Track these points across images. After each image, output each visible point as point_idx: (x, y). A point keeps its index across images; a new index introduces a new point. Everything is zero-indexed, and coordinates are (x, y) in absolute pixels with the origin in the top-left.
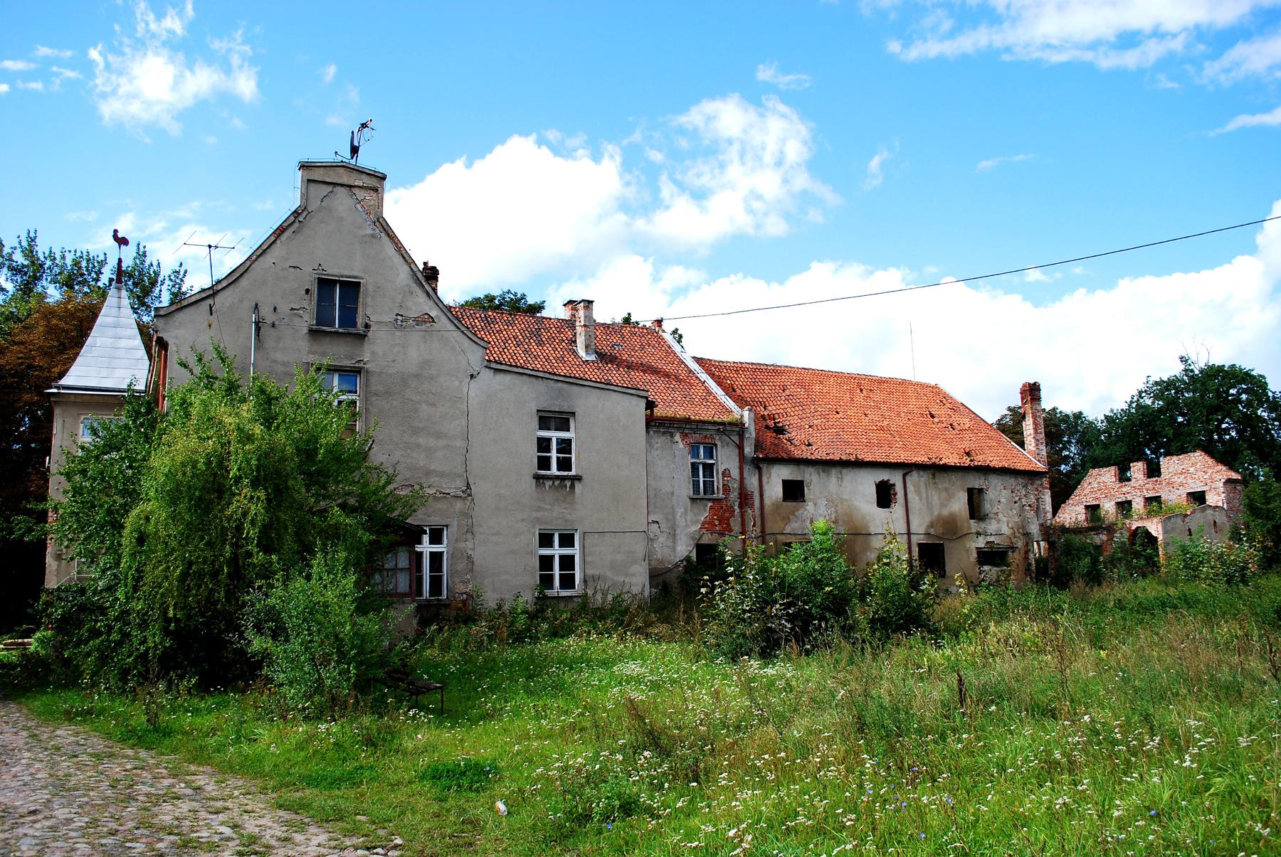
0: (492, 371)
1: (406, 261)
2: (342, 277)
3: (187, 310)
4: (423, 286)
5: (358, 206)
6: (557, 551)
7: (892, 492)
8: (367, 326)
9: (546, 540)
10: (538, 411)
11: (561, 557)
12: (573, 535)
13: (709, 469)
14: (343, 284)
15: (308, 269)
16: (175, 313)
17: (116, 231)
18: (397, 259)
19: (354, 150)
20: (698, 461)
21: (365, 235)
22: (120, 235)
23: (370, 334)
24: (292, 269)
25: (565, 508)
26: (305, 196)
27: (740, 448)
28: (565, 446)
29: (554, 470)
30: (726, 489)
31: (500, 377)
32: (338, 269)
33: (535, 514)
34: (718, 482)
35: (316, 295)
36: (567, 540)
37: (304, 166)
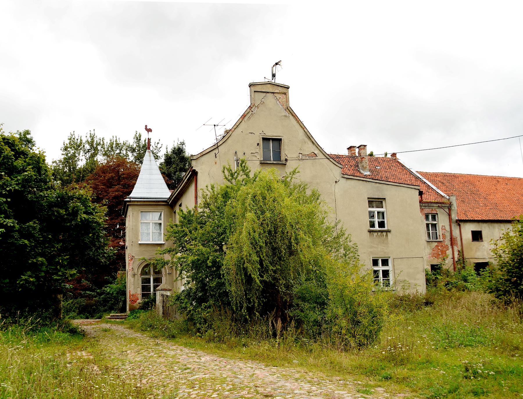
0: (345, 179)
1: (302, 127)
2: (273, 136)
4: (311, 139)
6: (380, 268)
8: (286, 160)
9: (375, 263)
11: (383, 271)
12: (388, 260)
13: (434, 226)
14: (273, 140)
15: (257, 134)
16: (200, 158)
17: (146, 126)
19: (274, 76)
20: (429, 222)
21: (282, 116)
22: (148, 128)
23: (288, 163)
24: (250, 134)
25: (384, 246)
27: (450, 215)
28: (382, 214)
29: (377, 228)
31: (349, 182)
32: (270, 134)
33: (370, 250)
34: (439, 233)
35: (262, 146)
36: (385, 262)
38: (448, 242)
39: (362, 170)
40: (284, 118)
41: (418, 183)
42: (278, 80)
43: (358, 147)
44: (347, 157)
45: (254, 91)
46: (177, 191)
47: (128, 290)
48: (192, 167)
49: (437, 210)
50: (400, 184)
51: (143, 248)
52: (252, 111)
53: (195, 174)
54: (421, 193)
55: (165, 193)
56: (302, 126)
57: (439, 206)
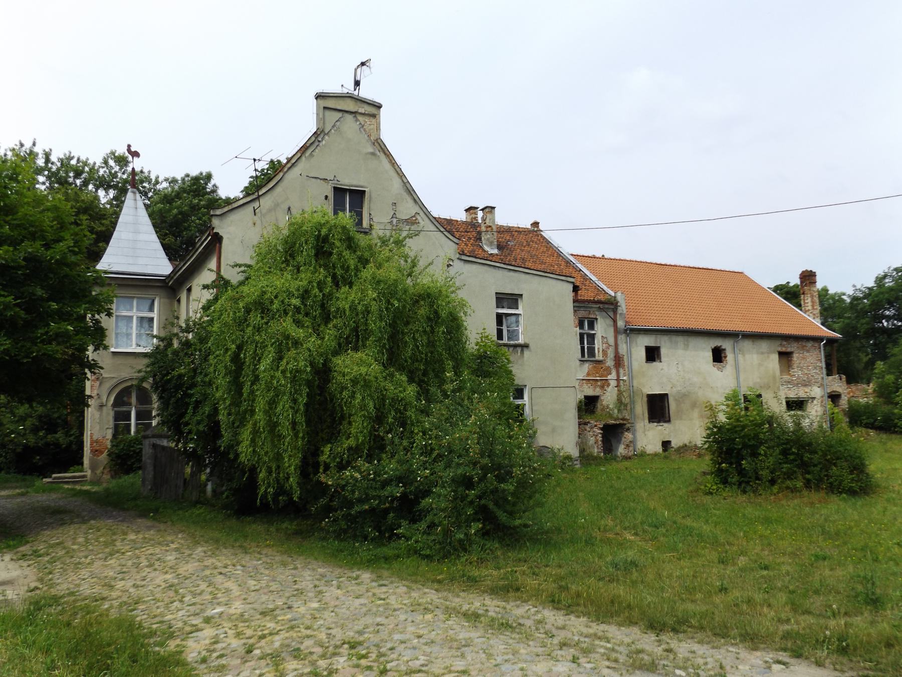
3: (236, 211)
5: (362, 130)
7: (723, 355)
10: (496, 293)
13: (592, 337)
14: (351, 191)
17: (129, 146)
18: (392, 173)
19: (357, 83)
20: (584, 332)
26: (321, 120)
27: (615, 321)
30: (605, 353)
31: (468, 266)
32: (348, 181)
37: (319, 96)
38: (610, 363)
39: (487, 245)
40: (370, 156)
41: (571, 270)
42: (365, 92)
43: (482, 210)
44: (463, 222)
45: (325, 108)
46: (184, 265)
47: (89, 433)
48: (213, 228)
49: (597, 313)
50: (546, 272)
51: (119, 360)
52: (319, 141)
53: (217, 239)
54: (576, 289)
55: (162, 266)
56: (399, 172)
57: (599, 307)
